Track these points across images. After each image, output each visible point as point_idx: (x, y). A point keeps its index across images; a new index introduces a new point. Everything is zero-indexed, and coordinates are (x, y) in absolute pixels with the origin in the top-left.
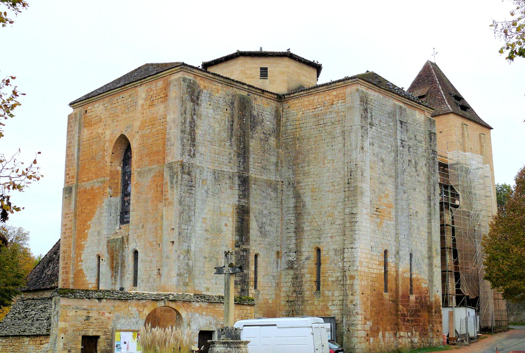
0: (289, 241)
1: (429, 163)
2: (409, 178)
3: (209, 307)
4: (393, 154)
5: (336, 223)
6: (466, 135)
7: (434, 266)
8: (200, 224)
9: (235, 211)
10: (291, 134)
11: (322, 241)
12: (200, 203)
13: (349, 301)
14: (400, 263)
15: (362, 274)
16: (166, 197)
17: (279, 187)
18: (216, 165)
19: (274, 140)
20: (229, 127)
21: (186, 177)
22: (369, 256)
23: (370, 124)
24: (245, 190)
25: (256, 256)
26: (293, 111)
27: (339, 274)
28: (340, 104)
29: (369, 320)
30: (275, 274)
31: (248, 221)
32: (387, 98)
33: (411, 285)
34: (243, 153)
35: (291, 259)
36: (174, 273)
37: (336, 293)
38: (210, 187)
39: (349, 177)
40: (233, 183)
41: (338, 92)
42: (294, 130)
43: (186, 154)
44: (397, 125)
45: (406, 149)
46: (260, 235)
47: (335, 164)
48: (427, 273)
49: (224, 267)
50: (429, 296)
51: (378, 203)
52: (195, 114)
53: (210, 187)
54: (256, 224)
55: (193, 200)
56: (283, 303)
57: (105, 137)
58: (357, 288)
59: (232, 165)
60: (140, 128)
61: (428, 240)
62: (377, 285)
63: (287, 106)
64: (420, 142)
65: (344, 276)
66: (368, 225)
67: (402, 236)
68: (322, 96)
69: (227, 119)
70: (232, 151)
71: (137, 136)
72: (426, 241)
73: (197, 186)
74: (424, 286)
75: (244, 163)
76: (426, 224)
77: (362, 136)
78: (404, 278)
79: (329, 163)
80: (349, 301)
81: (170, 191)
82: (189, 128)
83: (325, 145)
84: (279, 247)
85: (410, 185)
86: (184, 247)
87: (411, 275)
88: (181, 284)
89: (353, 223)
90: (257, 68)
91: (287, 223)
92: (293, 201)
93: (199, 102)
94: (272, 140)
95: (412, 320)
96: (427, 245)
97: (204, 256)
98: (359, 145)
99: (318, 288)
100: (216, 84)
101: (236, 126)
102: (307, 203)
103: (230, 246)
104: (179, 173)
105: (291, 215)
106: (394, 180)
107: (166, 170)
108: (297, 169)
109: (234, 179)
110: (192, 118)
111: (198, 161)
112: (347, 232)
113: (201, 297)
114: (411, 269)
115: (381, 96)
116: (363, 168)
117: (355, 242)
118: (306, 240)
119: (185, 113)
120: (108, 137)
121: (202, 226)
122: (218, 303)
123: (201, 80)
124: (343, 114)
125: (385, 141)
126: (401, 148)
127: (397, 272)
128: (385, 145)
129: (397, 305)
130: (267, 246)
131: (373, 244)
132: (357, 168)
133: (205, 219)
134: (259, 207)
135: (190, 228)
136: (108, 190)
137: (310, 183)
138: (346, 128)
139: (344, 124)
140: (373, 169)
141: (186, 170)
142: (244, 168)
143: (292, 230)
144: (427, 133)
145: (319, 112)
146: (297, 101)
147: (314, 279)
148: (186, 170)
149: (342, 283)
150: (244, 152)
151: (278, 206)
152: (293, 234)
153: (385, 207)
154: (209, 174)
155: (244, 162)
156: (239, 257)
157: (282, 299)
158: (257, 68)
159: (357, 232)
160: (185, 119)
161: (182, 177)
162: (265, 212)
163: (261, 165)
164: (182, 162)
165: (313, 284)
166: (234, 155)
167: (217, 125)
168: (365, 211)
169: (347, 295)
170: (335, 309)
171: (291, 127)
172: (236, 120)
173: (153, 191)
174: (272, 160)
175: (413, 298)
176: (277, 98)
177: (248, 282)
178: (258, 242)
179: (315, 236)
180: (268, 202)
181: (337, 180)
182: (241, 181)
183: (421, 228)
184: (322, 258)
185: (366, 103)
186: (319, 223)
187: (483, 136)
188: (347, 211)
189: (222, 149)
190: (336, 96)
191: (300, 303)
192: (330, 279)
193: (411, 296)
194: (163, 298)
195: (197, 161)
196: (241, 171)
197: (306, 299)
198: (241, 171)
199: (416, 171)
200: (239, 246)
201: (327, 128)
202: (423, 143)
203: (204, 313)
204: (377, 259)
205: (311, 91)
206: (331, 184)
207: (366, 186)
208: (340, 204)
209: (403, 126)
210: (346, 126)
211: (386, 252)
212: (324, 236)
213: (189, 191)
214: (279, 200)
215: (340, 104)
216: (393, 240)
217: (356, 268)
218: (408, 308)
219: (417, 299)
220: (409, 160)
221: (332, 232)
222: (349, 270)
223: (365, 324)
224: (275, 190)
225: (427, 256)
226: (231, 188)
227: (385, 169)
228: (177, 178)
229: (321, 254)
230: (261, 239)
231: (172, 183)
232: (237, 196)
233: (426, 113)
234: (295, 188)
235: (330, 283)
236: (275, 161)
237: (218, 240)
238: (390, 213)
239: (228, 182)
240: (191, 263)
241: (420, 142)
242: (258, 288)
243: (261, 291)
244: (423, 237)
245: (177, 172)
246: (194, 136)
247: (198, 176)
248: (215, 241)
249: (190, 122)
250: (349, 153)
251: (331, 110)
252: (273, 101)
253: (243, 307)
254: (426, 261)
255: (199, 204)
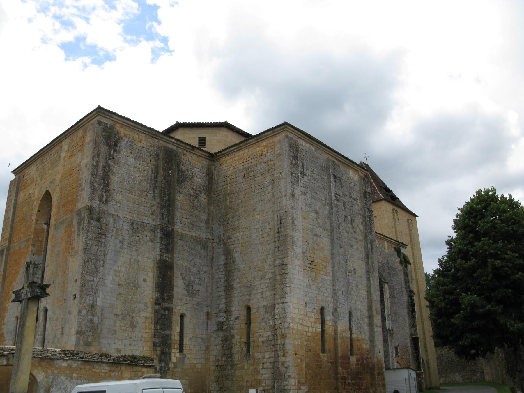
0: (219, 301)
1: (365, 221)
2: (346, 234)
3: (83, 367)
4: (327, 207)
5: (267, 278)
6: (396, 219)
7: (374, 326)
8: (111, 277)
9: (156, 265)
10: (223, 191)
11: (252, 298)
12: (113, 254)
13: (280, 364)
14: (338, 322)
15: (295, 331)
16: (73, 246)
17: (210, 245)
18: (135, 215)
19: (205, 197)
20: (153, 178)
21: (94, 223)
22: (303, 312)
23: (301, 173)
24: (168, 244)
25: (182, 317)
26: (225, 168)
27: (269, 333)
28: (269, 154)
29: (303, 384)
30: (204, 337)
31: (171, 278)
32: (319, 151)
33: (352, 346)
34: (168, 206)
35: (221, 319)
36: (74, 331)
37: (267, 355)
38: (126, 238)
39: (279, 226)
40: (155, 236)
41: (268, 142)
42: (225, 187)
43: (97, 198)
44: (330, 178)
45: (341, 204)
46: (187, 294)
47: (264, 215)
48: (368, 333)
49: (23, 288)
50: (371, 358)
51: (312, 255)
52: (110, 159)
53: (126, 238)
54: (182, 281)
55: (102, 249)
56: (213, 368)
57: (34, 196)
58: (289, 347)
59: (154, 217)
60: (61, 181)
61: (368, 298)
62: (313, 345)
63: (219, 164)
64: (356, 200)
65: (275, 335)
66: (301, 278)
67: (340, 292)
68: (252, 149)
69: (150, 170)
70: (155, 203)
71: (58, 190)
72: (366, 300)
73: (109, 235)
74: (365, 346)
75: (169, 215)
76: (365, 282)
77: (292, 182)
78: (343, 338)
79: (259, 214)
80: (280, 364)
81: (76, 239)
82: (102, 172)
83: (255, 197)
84: (209, 307)
85: (346, 240)
86: (88, 301)
87: (351, 335)
88: (82, 343)
89: (284, 275)
90: (195, 138)
91: (217, 281)
92: (223, 258)
93: (118, 149)
94: (203, 198)
95: (353, 384)
96: (366, 304)
97: (115, 313)
98: (289, 191)
99: (248, 351)
100: (140, 134)
101: (160, 178)
102: (237, 259)
103: (149, 303)
104: (86, 218)
105: (221, 273)
106: (330, 234)
107: (75, 217)
108: (228, 225)
109: (156, 232)
110: (107, 162)
111: (113, 209)
112: (278, 285)
113: (71, 354)
114: (350, 329)
115: (313, 148)
116: (294, 215)
117: (287, 296)
118: (236, 298)
119: (98, 156)
120: (36, 196)
121: (113, 279)
122: (97, 362)
123: (122, 127)
124: (272, 162)
125: (318, 192)
126: (336, 202)
127: (335, 330)
128: (319, 196)
129: (337, 367)
130: (195, 306)
131: (307, 299)
132: (287, 215)
133: (119, 272)
134: (186, 264)
135: (96, 280)
136: (31, 248)
137: (240, 238)
138: (275, 175)
139: (273, 173)
140: (305, 219)
141: (95, 216)
142: (168, 221)
143: (223, 288)
144: (362, 191)
145: (249, 165)
146: (229, 158)
147: (244, 340)
148: (95, 216)
149: (273, 343)
150: (169, 205)
151: (208, 264)
152: (222, 293)
153: (320, 261)
154: (125, 224)
155: (168, 215)
156: (160, 316)
157: (212, 363)
158: (195, 138)
159: (288, 285)
160: (98, 162)
161: (89, 223)
162: (194, 270)
163: (189, 221)
164: (90, 206)
165: (243, 346)
166: (157, 207)
167: (137, 175)
168: (297, 262)
169: (278, 357)
170: (265, 372)
171: (222, 184)
172: (161, 171)
173: (64, 242)
174: (202, 217)
175: (353, 359)
176: (209, 157)
177: (170, 344)
178: (184, 301)
179: (245, 293)
180: (197, 260)
181: (266, 231)
182: (164, 234)
183: (360, 286)
184: (252, 317)
185: (296, 151)
186: (249, 279)
187: (410, 221)
188: (278, 262)
189: (143, 200)
190: (265, 147)
191: (229, 367)
192: (261, 340)
193: (351, 357)
194: (6, 353)
195: (111, 208)
196: (165, 224)
197: (236, 362)
198: (165, 224)
199: (353, 227)
200: (159, 304)
201: (257, 179)
202: (359, 201)
203: (75, 375)
204: (313, 316)
205: (241, 145)
206: (260, 236)
207: (298, 236)
208: (270, 256)
209: (337, 181)
210: (276, 173)
211: (322, 309)
212: (254, 292)
213: (98, 239)
214: (209, 258)
215: (269, 154)
216: (331, 296)
217: (287, 325)
218: (349, 370)
219: (358, 360)
220: (345, 216)
221: (262, 287)
222: (280, 328)
223: (299, 389)
224: (206, 247)
225: (367, 315)
226: (153, 241)
227: (319, 221)
228: (84, 224)
229: (251, 312)
230: (188, 298)
231: (79, 230)
232: (158, 250)
233: (360, 173)
234: (225, 244)
235: (261, 344)
236: (206, 218)
237: (134, 296)
238: (325, 267)
239: (148, 234)
240: (96, 319)
241: (356, 200)
242: (184, 351)
243: (187, 355)
244: (362, 295)
245: (84, 217)
246: (108, 181)
247: (111, 225)
248: (130, 297)
249: (104, 167)
250: (279, 200)
251: (260, 161)
252: (204, 159)
253: (136, 368)
254: (366, 320)
255: (110, 255)
